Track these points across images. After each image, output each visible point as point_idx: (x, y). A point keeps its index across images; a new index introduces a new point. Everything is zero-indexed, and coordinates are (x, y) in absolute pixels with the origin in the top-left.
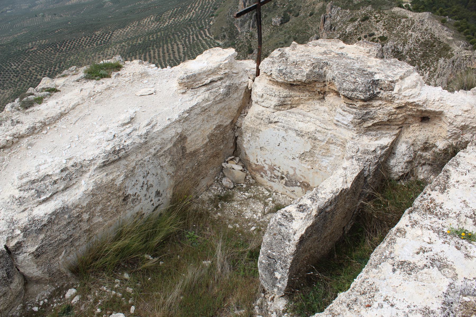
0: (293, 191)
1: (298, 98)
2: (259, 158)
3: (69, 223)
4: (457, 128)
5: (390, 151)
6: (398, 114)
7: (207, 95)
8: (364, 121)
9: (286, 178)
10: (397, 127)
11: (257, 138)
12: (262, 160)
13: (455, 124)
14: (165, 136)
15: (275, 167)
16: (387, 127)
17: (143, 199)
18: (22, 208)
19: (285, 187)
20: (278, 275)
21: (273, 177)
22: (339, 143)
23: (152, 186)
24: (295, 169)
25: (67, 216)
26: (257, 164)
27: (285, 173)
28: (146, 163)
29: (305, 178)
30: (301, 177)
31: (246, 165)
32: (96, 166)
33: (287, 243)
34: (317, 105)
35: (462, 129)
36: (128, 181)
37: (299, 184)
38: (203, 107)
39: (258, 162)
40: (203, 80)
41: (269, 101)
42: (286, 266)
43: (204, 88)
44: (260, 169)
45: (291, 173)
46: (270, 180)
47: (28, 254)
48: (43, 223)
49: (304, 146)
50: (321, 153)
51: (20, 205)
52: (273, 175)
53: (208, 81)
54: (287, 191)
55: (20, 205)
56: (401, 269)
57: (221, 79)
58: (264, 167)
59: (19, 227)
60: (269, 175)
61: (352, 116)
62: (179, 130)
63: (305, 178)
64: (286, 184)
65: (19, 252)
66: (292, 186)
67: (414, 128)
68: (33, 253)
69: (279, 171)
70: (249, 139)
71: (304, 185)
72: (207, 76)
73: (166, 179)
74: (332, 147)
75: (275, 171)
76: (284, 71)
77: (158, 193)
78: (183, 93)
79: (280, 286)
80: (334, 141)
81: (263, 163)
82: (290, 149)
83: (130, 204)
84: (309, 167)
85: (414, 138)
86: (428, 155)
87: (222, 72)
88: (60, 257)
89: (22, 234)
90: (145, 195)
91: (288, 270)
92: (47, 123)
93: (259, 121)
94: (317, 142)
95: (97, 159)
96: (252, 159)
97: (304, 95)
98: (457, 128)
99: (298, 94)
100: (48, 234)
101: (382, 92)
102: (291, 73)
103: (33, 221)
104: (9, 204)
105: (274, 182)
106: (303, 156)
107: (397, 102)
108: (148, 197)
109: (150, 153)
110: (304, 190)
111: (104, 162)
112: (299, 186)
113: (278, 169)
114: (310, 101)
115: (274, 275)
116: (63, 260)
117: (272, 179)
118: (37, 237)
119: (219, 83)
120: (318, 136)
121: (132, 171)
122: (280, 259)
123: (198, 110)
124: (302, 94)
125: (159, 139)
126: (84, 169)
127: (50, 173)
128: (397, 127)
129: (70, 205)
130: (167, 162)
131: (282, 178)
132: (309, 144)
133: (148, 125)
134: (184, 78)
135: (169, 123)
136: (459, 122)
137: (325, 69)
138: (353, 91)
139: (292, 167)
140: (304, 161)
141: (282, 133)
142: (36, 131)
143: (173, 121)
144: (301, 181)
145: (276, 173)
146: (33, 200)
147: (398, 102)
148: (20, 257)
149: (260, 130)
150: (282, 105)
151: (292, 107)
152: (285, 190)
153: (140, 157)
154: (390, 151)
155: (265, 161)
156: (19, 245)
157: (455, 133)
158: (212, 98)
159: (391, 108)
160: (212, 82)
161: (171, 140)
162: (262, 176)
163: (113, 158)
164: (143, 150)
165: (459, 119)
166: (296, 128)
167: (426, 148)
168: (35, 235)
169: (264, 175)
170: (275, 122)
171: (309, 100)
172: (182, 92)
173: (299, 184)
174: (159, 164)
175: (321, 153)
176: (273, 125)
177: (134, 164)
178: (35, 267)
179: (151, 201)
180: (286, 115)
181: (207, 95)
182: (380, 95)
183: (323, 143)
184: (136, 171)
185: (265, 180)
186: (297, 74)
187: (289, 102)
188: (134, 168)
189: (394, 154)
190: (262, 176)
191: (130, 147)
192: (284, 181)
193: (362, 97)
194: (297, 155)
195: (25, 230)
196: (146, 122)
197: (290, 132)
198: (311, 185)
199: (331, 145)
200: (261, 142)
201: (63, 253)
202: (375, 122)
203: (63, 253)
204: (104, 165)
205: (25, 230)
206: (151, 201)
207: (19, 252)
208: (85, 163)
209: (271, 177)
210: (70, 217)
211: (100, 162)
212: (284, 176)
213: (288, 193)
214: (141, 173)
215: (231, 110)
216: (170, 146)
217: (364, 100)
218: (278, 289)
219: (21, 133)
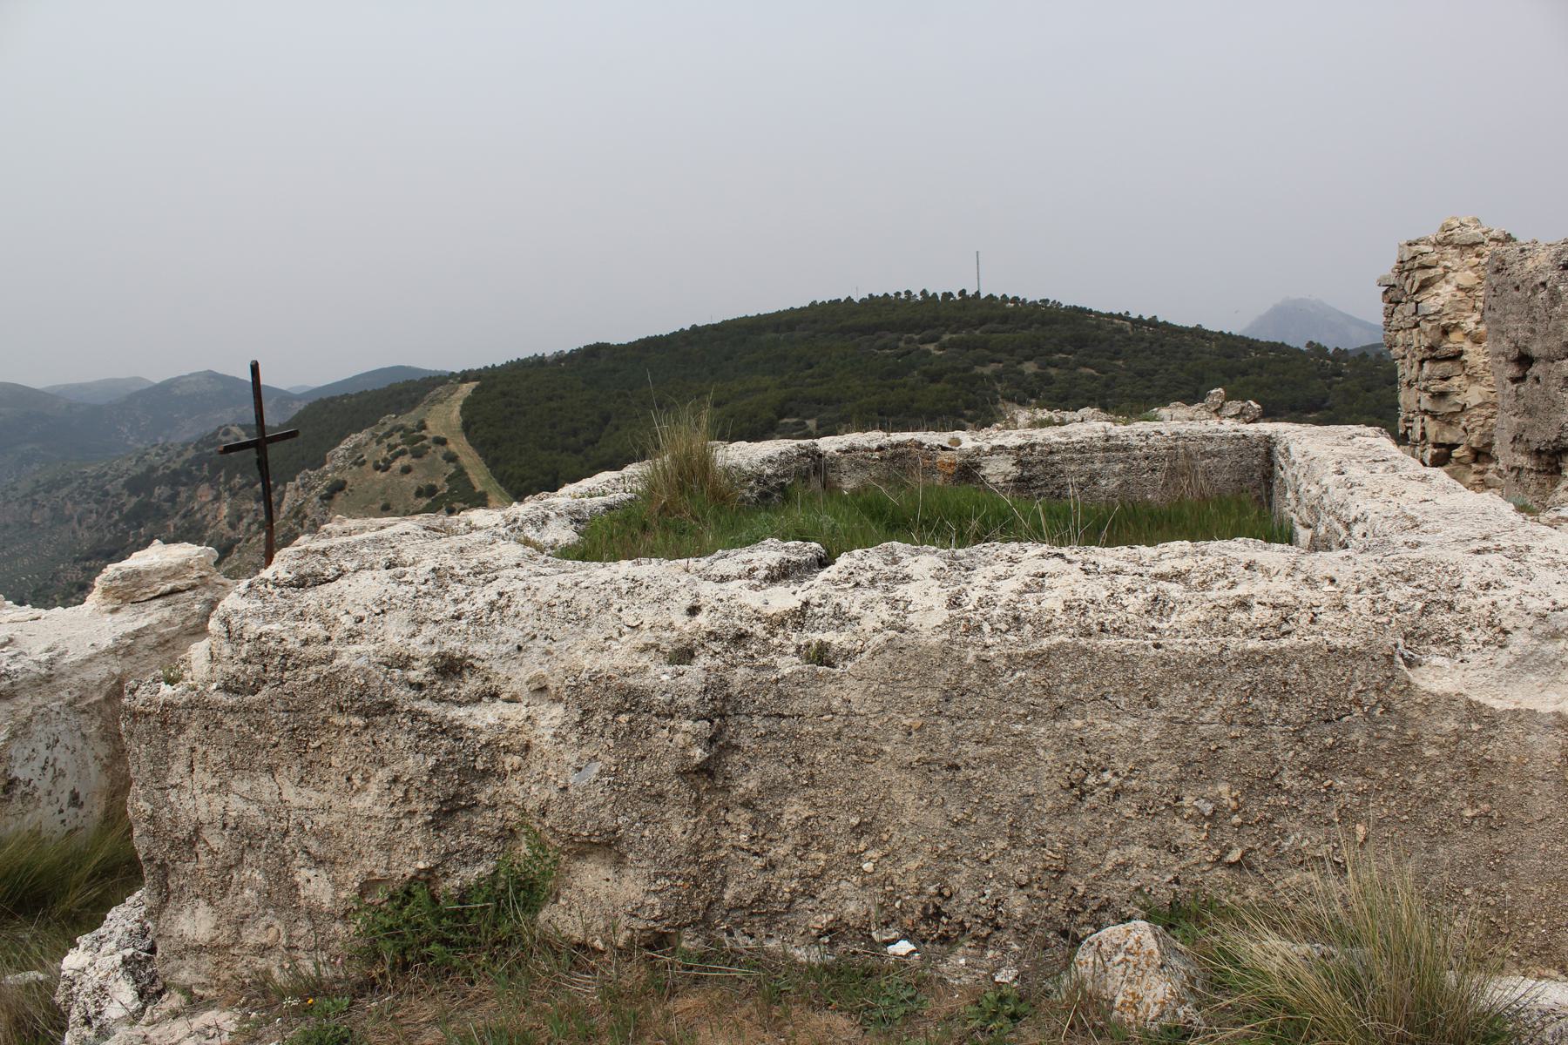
7: (167, 612)
14: (87, 676)
17: (45, 800)
23: (62, 774)
28: (53, 715)
36: (16, 745)
38: (162, 635)
40: (156, 586)
43: (159, 602)
53: (168, 587)
56: (409, 732)
57: (193, 587)
62: (117, 670)
72: (163, 579)
73: (94, 768)
77: (75, 800)
78: (114, 611)
83: (16, 805)
87: (195, 574)
90: (49, 794)
108: (53, 798)
109: (61, 698)
119: (189, 594)
121: (25, 725)
123: (151, 640)
125: (75, 679)
130: (93, 729)
133: (49, 650)
143: (103, 648)
153: (39, 700)
158: (178, 620)
160: (173, 592)
161: (99, 687)
164: (45, 688)
172: (110, 607)
174: (79, 727)
177: (28, 712)
179: (61, 811)
184: (33, 727)
188: (30, 719)
191: (21, 677)
196: (44, 646)
206: (61, 811)
214: (43, 735)
216: (97, 697)
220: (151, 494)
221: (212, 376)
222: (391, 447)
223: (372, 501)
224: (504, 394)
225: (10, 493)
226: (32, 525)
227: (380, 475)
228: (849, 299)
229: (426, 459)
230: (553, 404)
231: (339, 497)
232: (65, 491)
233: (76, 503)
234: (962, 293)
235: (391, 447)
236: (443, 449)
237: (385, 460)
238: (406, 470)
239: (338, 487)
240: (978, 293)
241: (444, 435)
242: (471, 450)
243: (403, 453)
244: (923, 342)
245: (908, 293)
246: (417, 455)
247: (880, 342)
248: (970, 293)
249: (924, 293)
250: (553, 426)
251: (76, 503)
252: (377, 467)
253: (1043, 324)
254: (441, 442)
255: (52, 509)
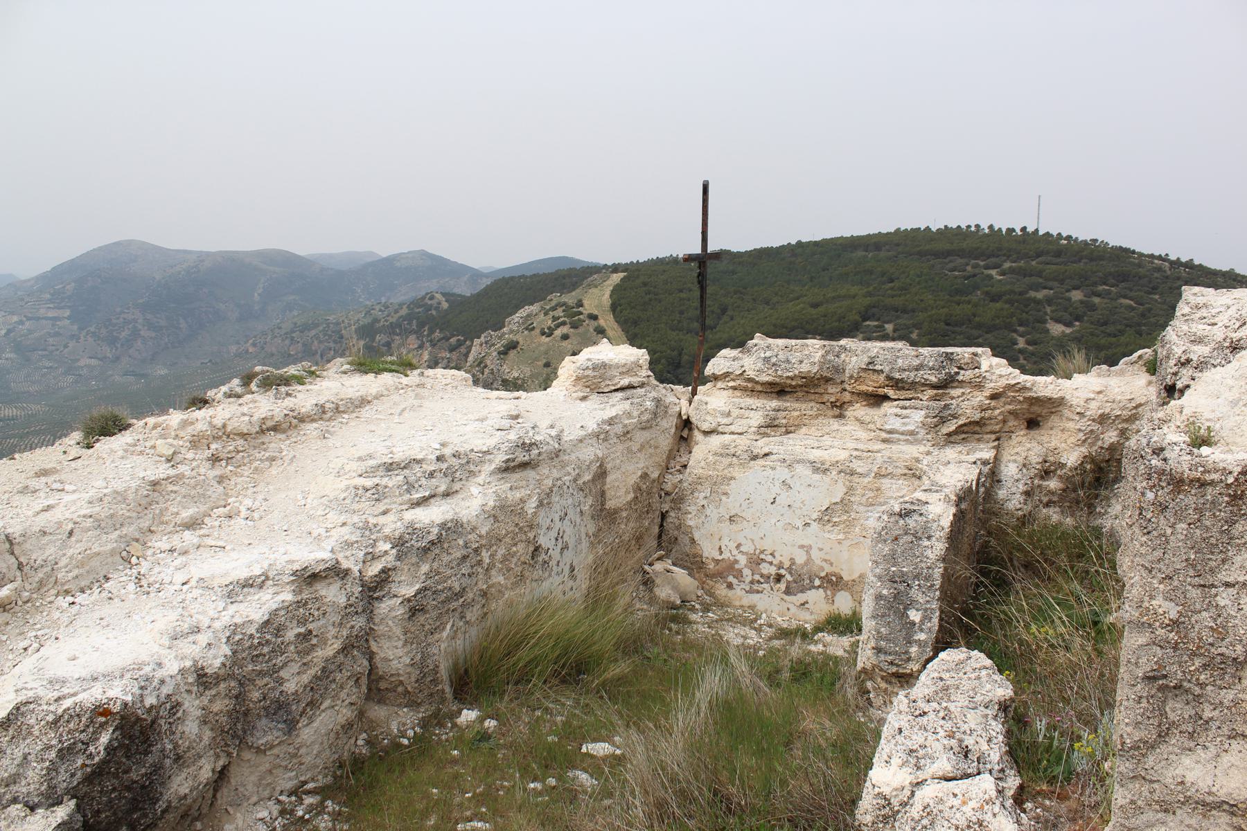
0: (803, 605)
1: (798, 413)
2: (725, 541)
3: (465, 558)
4: (1094, 420)
5: (992, 476)
6: (995, 408)
8: (943, 421)
9: (789, 577)
10: (993, 437)
11: (724, 498)
12: (732, 545)
13: (1088, 413)
15: (762, 556)
16: (977, 436)
18: (382, 507)
19: (786, 597)
20: (915, 616)
21: (758, 582)
22: (900, 471)
24: (807, 549)
25: (461, 542)
26: (720, 558)
27: (787, 564)
29: (831, 564)
30: (824, 564)
31: (694, 564)
32: (493, 466)
33: (926, 543)
34: (835, 424)
35: (1100, 423)
37: (817, 582)
39: (721, 553)
40: (616, 380)
41: (744, 421)
42: (932, 585)
43: (620, 395)
44: (727, 570)
45: (800, 558)
46: (750, 591)
47: (400, 600)
48: (431, 537)
49: (830, 490)
50: (864, 499)
51: (377, 500)
52: (757, 577)
54: (790, 606)
55: (377, 500)
58: (736, 562)
59: (386, 537)
60: (748, 579)
61: (923, 413)
63: (831, 564)
64: (788, 592)
65: (382, 593)
66: (802, 592)
67: (1019, 439)
68: (409, 600)
69: (771, 563)
70: (704, 502)
71: (830, 581)
74: (886, 483)
75: (764, 565)
76: (774, 360)
78: (584, 398)
79: (922, 636)
80: (890, 469)
81: (735, 552)
82: (798, 504)
84: (841, 536)
85: (1024, 455)
86: (1053, 484)
88: (445, 634)
89: (394, 551)
91: (938, 593)
92: (341, 409)
93: (726, 461)
94: (855, 479)
95: (495, 452)
96: (708, 551)
97: (809, 407)
98: (1094, 420)
99: (797, 405)
100: (435, 565)
101: (962, 372)
102: (788, 361)
103: (412, 529)
104: (347, 501)
105: (758, 592)
106: (826, 516)
107: (990, 388)
110: (829, 593)
111: (508, 460)
112: (819, 587)
113: (770, 558)
114: (820, 419)
115: (908, 617)
116: (449, 644)
117: (755, 587)
118: (417, 565)
119: (640, 391)
120: (859, 466)
121: (548, 495)
122: (917, 577)
124: (804, 406)
126: (472, 467)
127: (419, 457)
128: (993, 437)
129: (465, 520)
131: (779, 578)
132: (840, 484)
134: (587, 368)
135: (583, 433)
136: (1094, 409)
137: (843, 356)
138: (917, 370)
139: (802, 547)
140: (828, 527)
141: (783, 473)
142: (326, 416)
144: (823, 574)
145: (766, 569)
146: (401, 495)
147: (992, 385)
148: (383, 605)
149: (732, 478)
150: (770, 426)
151: (788, 432)
152: (786, 606)
154: (992, 476)
155: (738, 546)
156: (385, 577)
157: (1092, 431)
159: (980, 398)
162: (730, 586)
163: (522, 457)
165: (1093, 405)
166: (811, 458)
167: (1046, 474)
168: (414, 560)
169: (735, 581)
170: (766, 455)
171: (817, 417)
173: (817, 582)
175: (864, 499)
176: (761, 462)
178: (400, 643)
180: (782, 443)
181: (626, 405)
182: (960, 378)
183: (866, 480)
185: (739, 596)
186: (801, 362)
187: (784, 421)
189: (999, 481)
190: (730, 586)
192: (782, 586)
193: (934, 379)
194: (815, 516)
195: (399, 543)
197: (799, 469)
198: (846, 578)
199: (883, 481)
200: (732, 504)
201: (448, 627)
202: (960, 423)
203: (448, 627)
204: (506, 470)
205: (399, 543)
207: (382, 593)
208: (472, 456)
209: (752, 582)
210: (466, 546)
211: (499, 459)
212: (783, 572)
213: (793, 610)
215: (658, 451)
217: (934, 387)
218: (920, 646)
219: (303, 410)
220: (374, 340)
221: (424, 254)
222: (555, 318)
223: (537, 359)
224: (645, 284)
225: (277, 331)
226: (289, 355)
227: (544, 339)
228: (928, 228)
229: (581, 330)
230: (683, 295)
231: (512, 353)
232: (313, 332)
233: (320, 342)
234: (1024, 229)
235: (555, 318)
236: (594, 324)
237: (549, 328)
238: (565, 337)
239: (513, 346)
240: (1037, 230)
241: (596, 312)
242: (616, 326)
243: (564, 323)
244: (987, 267)
245: (977, 226)
246: (575, 326)
247: (951, 265)
248: (1030, 229)
249: (991, 227)
250: (681, 313)
251: (320, 342)
252: (543, 333)
253: (1092, 260)
254: (594, 317)
255: (304, 345)
